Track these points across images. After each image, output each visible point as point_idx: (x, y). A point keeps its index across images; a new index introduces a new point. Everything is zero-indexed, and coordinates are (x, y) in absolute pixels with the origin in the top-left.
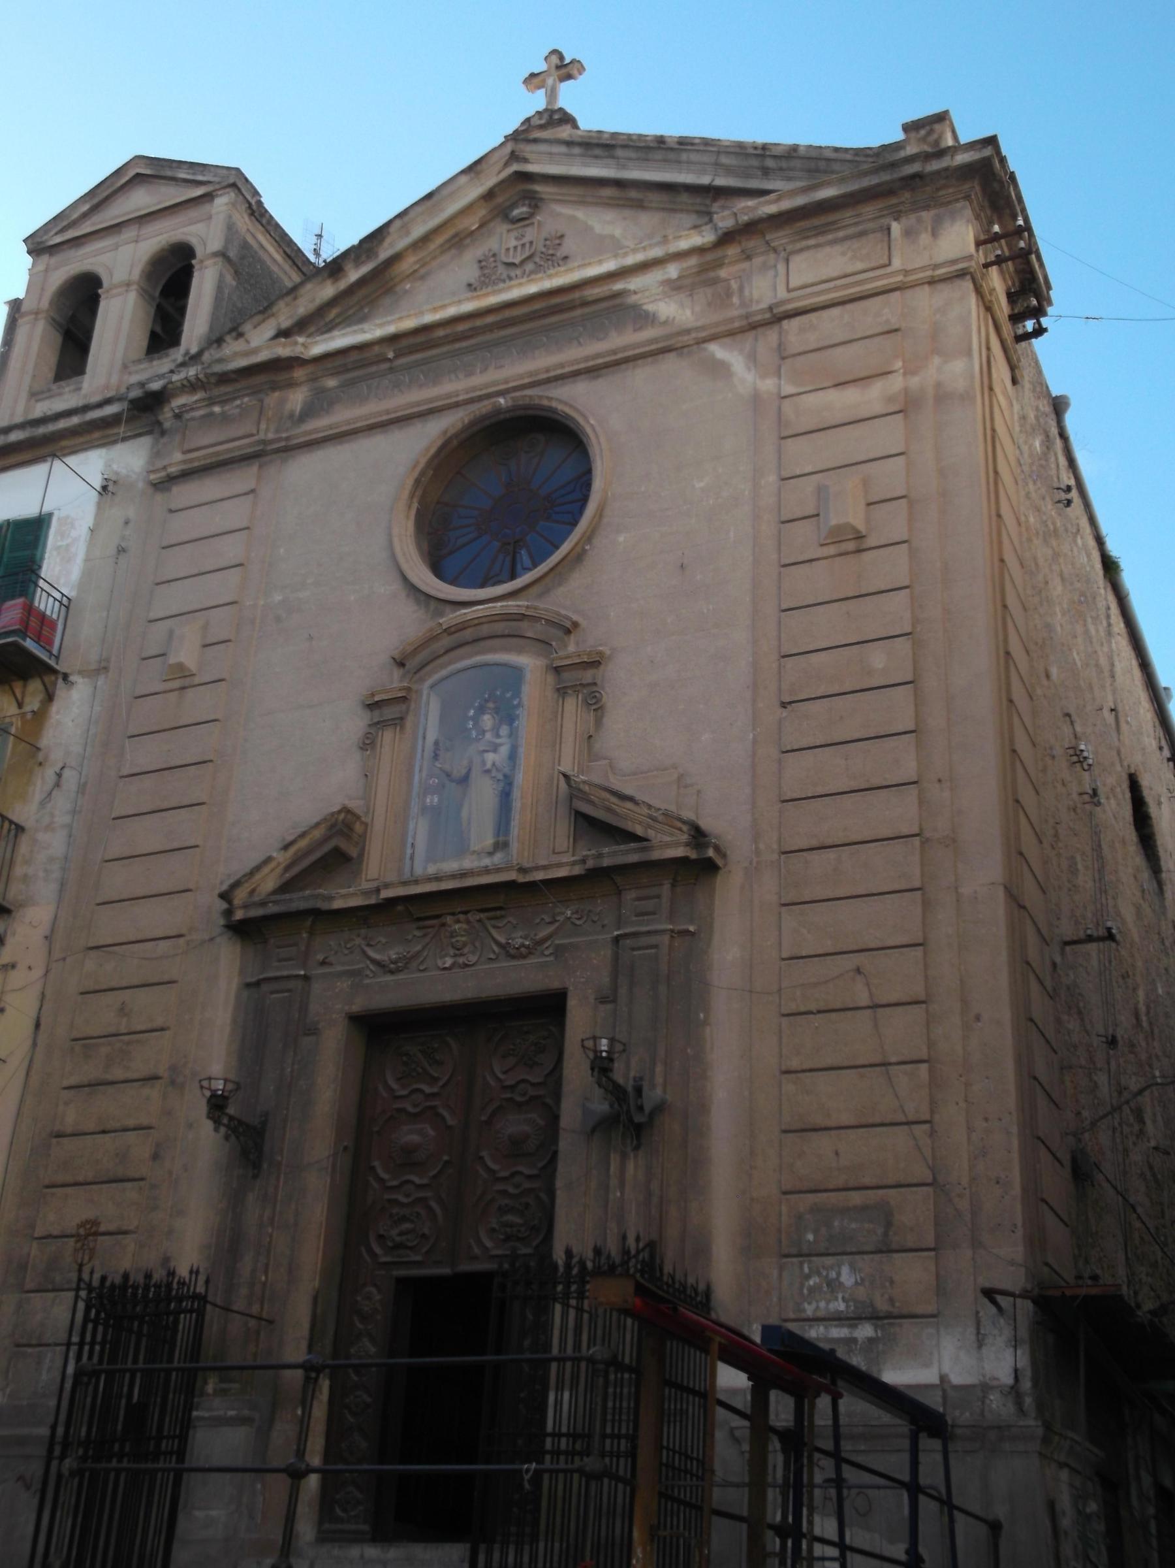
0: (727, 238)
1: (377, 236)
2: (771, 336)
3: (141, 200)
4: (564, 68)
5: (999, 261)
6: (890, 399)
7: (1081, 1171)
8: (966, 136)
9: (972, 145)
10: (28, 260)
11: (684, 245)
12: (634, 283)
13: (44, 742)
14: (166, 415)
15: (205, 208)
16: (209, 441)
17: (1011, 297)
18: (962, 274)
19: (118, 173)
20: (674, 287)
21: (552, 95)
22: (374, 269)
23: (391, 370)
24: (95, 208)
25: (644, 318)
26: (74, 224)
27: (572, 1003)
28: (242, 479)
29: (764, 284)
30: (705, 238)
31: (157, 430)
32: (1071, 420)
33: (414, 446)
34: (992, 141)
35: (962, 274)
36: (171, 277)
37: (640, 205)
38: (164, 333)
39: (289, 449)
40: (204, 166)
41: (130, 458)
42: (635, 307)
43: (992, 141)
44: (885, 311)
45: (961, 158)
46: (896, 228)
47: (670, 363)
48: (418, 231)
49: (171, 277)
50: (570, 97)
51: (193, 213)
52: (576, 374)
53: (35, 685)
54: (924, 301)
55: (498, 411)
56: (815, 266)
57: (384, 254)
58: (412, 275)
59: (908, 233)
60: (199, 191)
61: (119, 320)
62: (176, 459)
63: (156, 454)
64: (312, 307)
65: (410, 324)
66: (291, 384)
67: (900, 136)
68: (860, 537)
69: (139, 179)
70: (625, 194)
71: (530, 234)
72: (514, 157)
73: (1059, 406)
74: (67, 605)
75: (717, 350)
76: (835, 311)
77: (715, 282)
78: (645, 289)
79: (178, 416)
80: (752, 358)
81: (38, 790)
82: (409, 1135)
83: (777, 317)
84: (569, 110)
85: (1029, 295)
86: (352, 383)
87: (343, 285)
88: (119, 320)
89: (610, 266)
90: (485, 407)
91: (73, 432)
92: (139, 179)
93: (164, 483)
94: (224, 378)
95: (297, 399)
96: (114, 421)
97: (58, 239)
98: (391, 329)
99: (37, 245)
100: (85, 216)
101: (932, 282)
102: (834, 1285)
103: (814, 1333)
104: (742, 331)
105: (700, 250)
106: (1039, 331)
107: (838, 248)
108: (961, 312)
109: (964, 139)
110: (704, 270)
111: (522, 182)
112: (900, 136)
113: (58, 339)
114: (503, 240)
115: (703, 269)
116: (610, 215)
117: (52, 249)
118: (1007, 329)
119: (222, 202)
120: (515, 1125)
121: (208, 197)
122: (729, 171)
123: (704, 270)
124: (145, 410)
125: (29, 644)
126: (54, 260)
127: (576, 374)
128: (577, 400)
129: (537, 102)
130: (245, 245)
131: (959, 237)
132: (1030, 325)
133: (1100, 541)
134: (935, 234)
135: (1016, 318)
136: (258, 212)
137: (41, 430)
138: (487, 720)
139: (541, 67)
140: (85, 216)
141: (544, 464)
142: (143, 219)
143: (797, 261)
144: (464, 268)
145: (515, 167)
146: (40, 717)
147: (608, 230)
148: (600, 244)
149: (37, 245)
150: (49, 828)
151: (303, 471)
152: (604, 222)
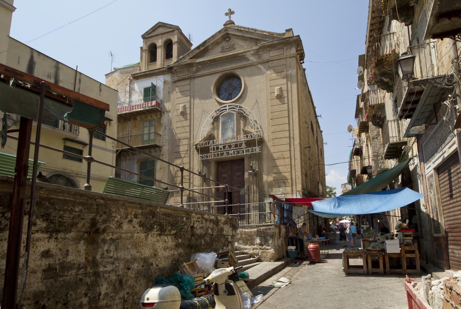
0: (260, 48)
1: (205, 42)
2: (267, 64)
3: (161, 30)
4: (231, 13)
5: (299, 54)
6: (284, 75)
7: (306, 175)
8: (295, 34)
9: (296, 36)
10: (142, 40)
11: (254, 48)
12: (247, 54)
13: (162, 122)
14: (173, 70)
15: (173, 33)
16: (181, 76)
17: (300, 57)
18: (294, 56)
19: (156, 25)
20: (252, 55)
21: (230, 17)
22: (205, 48)
23: (209, 65)
24: (153, 31)
25: (248, 60)
26: (149, 34)
27: (245, 159)
28: (188, 82)
29: (266, 56)
30: (257, 48)
31: (171, 72)
32: (306, 72)
33: (215, 78)
34: (299, 36)
35: (294, 56)
36: (168, 45)
37: (246, 40)
38: (169, 55)
39: (194, 78)
40: (172, 25)
41: (168, 77)
42: (247, 57)
43: (299, 36)
44: (283, 62)
45: (294, 38)
46: (285, 48)
47: (252, 67)
48: (211, 42)
49: (168, 45)
50: (233, 18)
51: (171, 34)
52: (238, 68)
53: (158, 113)
54: (288, 60)
55: (227, 73)
56: (273, 54)
57: (206, 45)
58: (211, 49)
59: (286, 49)
60: (171, 30)
61: (160, 53)
62: (176, 78)
63: (172, 77)
64: (195, 54)
65: (212, 58)
66: (193, 67)
67: (285, 32)
68: (281, 96)
69: (160, 26)
70: (244, 38)
71: (229, 43)
72: (226, 30)
73: (304, 70)
74: (161, 101)
75: (259, 66)
76: (276, 61)
77: (259, 54)
78: (248, 55)
79: (175, 71)
80: (264, 67)
81: (162, 130)
82: (224, 175)
83: (268, 61)
84: (233, 21)
85: (301, 56)
86: (203, 67)
87: (200, 50)
88: (160, 53)
89: (243, 51)
90: (225, 72)
91: (158, 72)
92: (160, 26)
93: (175, 82)
94: (182, 66)
95: (194, 69)
96: (165, 71)
97: (147, 36)
98: (209, 59)
99: (144, 37)
100: (151, 32)
101: (290, 57)
102: (280, 191)
103: (277, 196)
104: (263, 63)
105: (257, 49)
106: (303, 62)
107: (277, 51)
108: (293, 62)
109: (295, 35)
110: (257, 53)
111: (227, 34)
112: (285, 32)
113: (150, 54)
114: (225, 44)
115: (257, 52)
116: (242, 41)
117: (147, 38)
118: (299, 61)
119: (176, 32)
120: (238, 174)
121: (173, 31)
122: (260, 37)
123: (257, 53)
124: (170, 70)
125: (157, 108)
126: (147, 40)
127: (238, 68)
128: (238, 72)
129: (227, 19)
130: (180, 39)
131: (293, 51)
132: (302, 61)
133: (308, 88)
134: (290, 49)
135: (300, 60)
136: (181, 33)
137: (152, 72)
138: (229, 120)
139: (227, 12)
140: (151, 32)
141: (235, 82)
142: (162, 34)
143: (271, 52)
144: (219, 49)
145: (226, 32)
146: (160, 118)
147: (241, 44)
148: (241, 47)
149: (144, 37)
150: (165, 135)
151: (197, 81)
152: (241, 43)
